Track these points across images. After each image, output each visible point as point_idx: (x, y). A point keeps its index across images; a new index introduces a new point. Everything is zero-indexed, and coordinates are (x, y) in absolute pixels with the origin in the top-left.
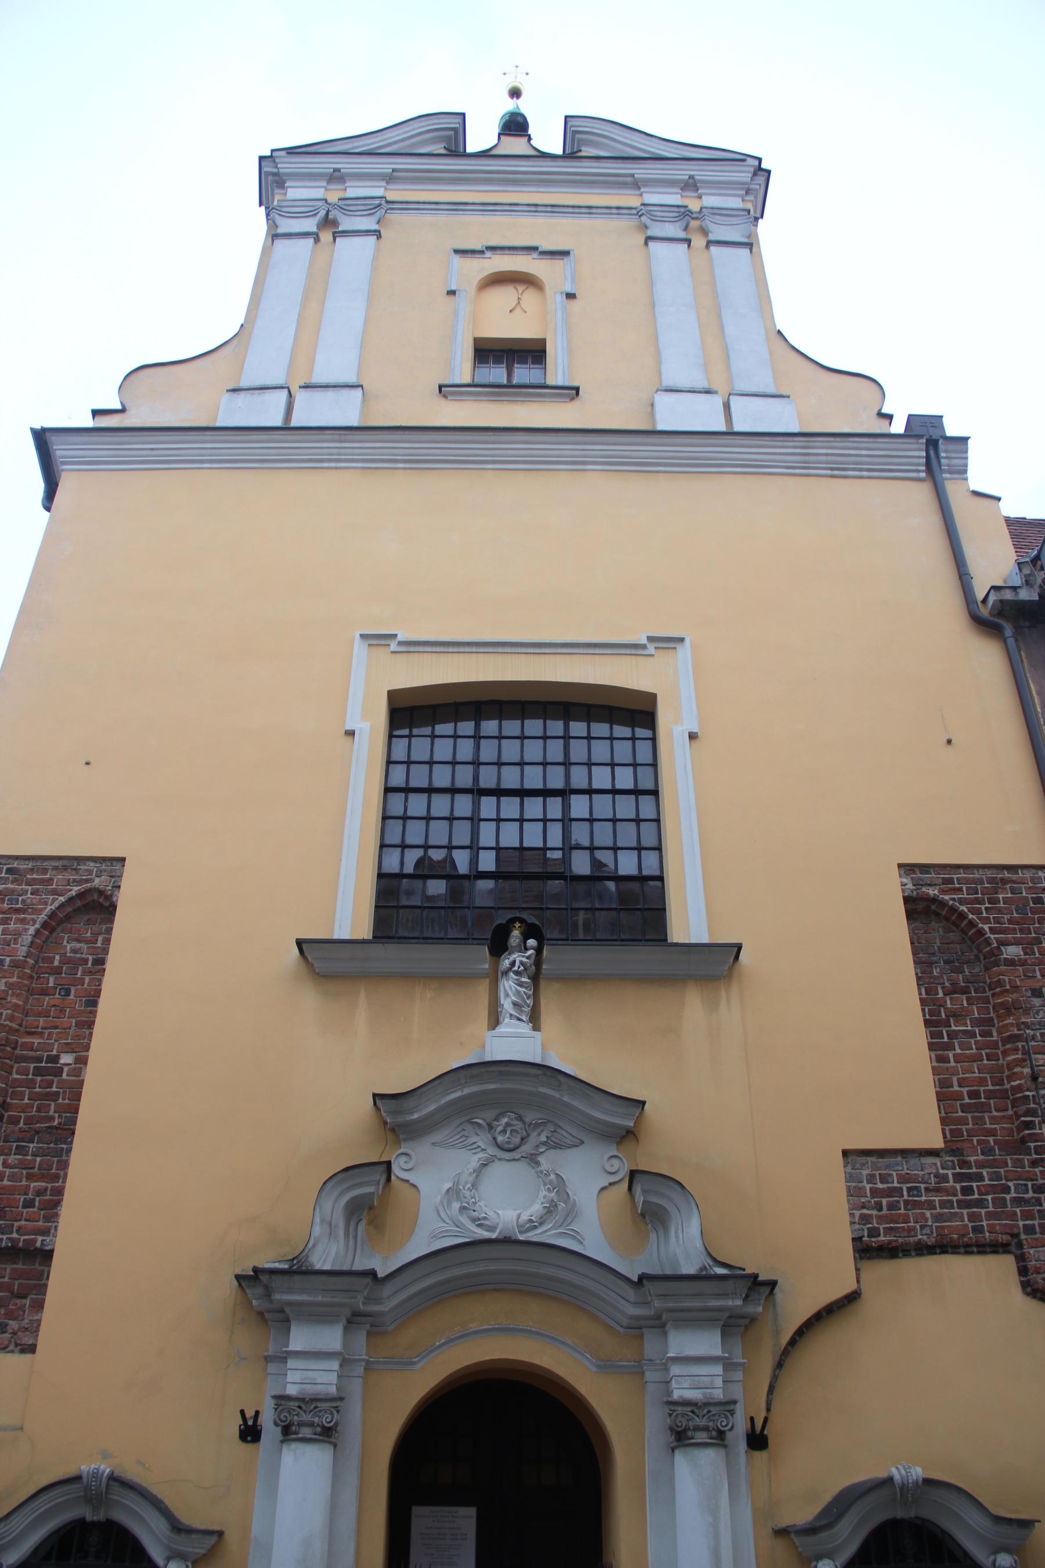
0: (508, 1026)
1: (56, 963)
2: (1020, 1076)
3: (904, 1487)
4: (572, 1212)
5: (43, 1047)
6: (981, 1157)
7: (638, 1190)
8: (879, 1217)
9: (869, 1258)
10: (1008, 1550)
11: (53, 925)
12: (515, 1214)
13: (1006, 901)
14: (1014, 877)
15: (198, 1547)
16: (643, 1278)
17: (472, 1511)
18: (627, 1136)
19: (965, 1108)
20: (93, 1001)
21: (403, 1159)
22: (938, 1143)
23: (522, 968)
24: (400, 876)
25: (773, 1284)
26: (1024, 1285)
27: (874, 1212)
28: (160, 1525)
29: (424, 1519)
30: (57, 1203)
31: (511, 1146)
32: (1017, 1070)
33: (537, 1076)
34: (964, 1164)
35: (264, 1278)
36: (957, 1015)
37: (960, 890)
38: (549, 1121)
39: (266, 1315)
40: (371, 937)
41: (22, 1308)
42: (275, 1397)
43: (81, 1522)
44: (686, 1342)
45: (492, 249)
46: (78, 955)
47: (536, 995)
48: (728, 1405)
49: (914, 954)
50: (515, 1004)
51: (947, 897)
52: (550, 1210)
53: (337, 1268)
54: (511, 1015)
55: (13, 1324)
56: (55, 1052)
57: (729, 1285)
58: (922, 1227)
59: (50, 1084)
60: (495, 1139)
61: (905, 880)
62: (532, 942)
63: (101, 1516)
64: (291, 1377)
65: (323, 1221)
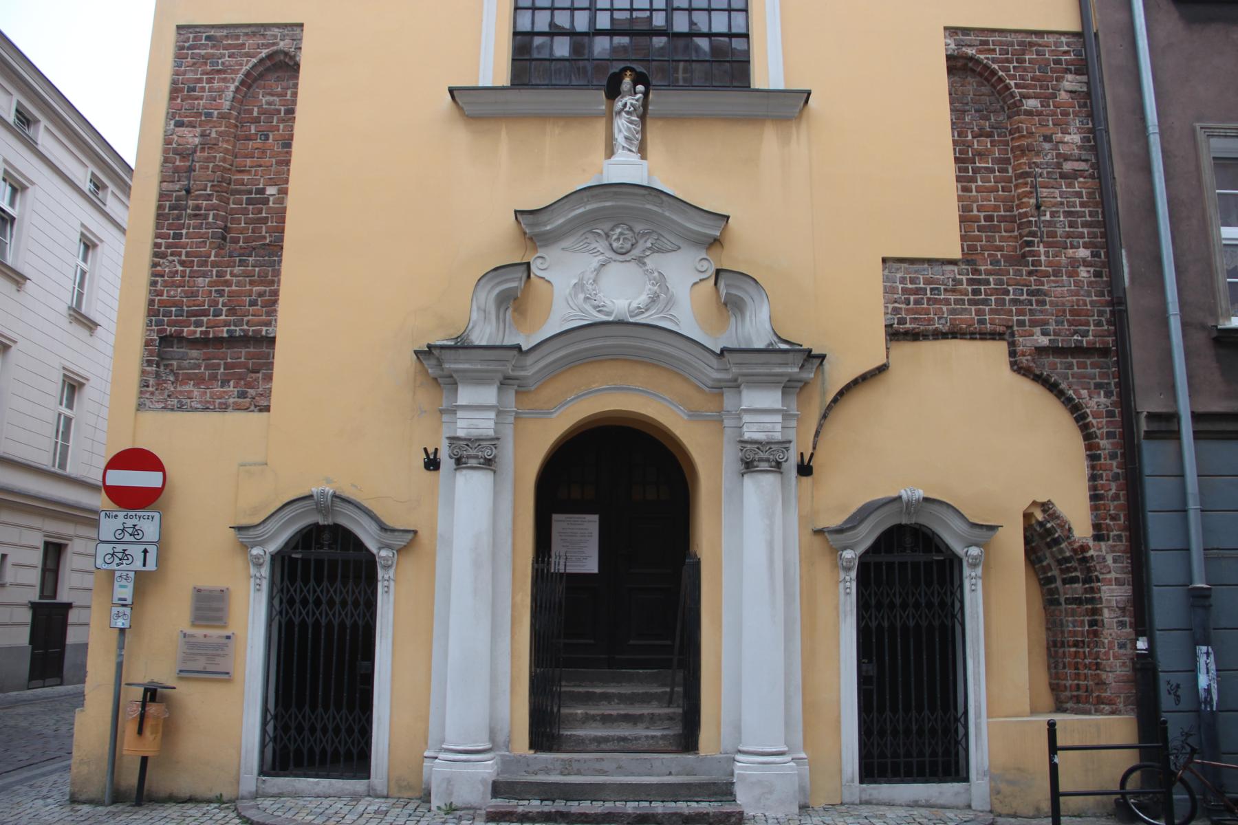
0: (621, 156)
1: (255, 114)
2: (1027, 205)
3: (909, 503)
4: (671, 302)
6: (990, 267)
7: (722, 284)
8: (907, 310)
9: (898, 340)
10: (977, 545)
11: (249, 82)
12: (627, 302)
13: (1031, 61)
14: (1040, 41)
15: (401, 541)
16: (724, 351)
17: (596, 518)
18: (715, 243)
19: (980, 229)
20: (287, 144)
21: (540, 261)
22: (957, 254)
24: (533, 34)
26: (1012, 364)
27: (903, 306)
28: (373, 527)
29: (561, 523)
30: (275, 302)
32: (1025, 200)
33: (644, 196)
34: (976, 272)
35: (436, 352)
36: (981, 155)
37: (994, 50)
40: (509, 84)
41: (256, 380)
42: (449, 438)
43: (317, 525)
44: (753, 398)
48: (785, 444)
49: (951, 103)
50: (626, 138)
51: (982, 57)
52: (654, 299)
53: (491, 344)
55: (251, 392)
57: (790, 356)
58: (939, 319)
59: (260, 212)
61: (949, 41)
62: (640, 88)
63: (329, 521)
64: (460, 424)
65: (479, 308)
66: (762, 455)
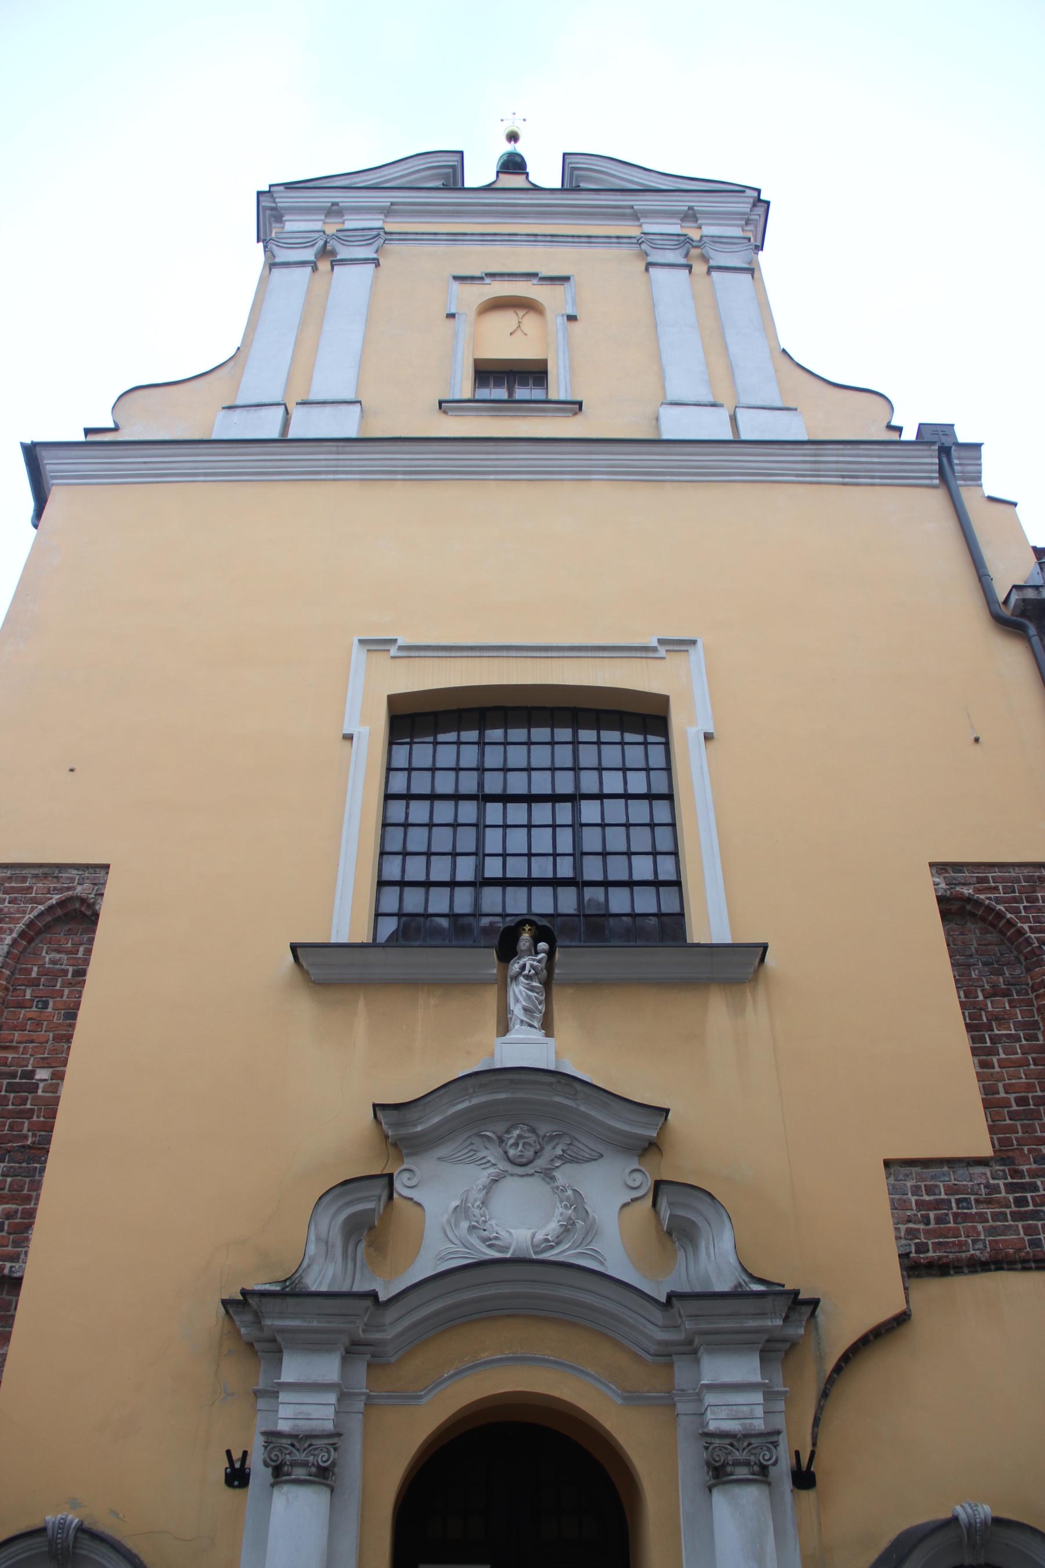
1: (34, 975)
3: (971, 1527)
4: (591, 1231)
5: (17, 1062)
6: (1034, 1166)
9: (919, 1276)
11: (31, 934)
12: (528, 1233)
18: (649, 1148)
19: (1012, 1116)
20: (72, 1015)
21: (406, 1175)
22: (986, 1150)
23: (533, 972)
25: (815, 1303)
27: (921, 1226)
30: (29, 1226)
31: (524, 1160)
33: (551, 1084)
34: (1016, 1173)
35: (253, 1301)
36: (999, 1019)
37: (996, 888)
38: (564, 1134)
39: (257, 1345)
42: (265, 1434)
45: (492, 275)
46: (58, 967)
47: (548, 1001)
48: (771, 1437)
49: (951, 957)
51: (982, 897)
52: (568, 1228)
53: (336, 1289)
54: (522, 1021)
56: (30, 1068)
57: (768, 1303)
58: (974, 1242)
60: (506, 1153)
61: (937, 880)
62: (543, 945)
64: (284, 1411)
65: (318, 1239)
66: (738, 1455)
